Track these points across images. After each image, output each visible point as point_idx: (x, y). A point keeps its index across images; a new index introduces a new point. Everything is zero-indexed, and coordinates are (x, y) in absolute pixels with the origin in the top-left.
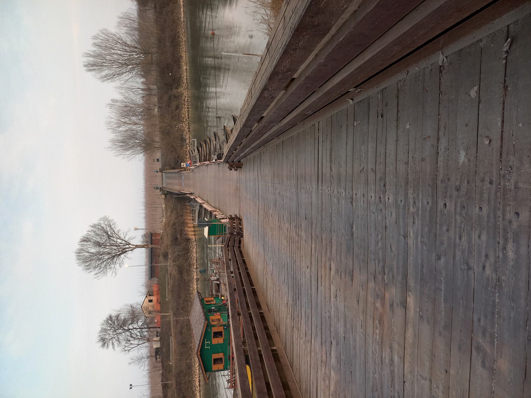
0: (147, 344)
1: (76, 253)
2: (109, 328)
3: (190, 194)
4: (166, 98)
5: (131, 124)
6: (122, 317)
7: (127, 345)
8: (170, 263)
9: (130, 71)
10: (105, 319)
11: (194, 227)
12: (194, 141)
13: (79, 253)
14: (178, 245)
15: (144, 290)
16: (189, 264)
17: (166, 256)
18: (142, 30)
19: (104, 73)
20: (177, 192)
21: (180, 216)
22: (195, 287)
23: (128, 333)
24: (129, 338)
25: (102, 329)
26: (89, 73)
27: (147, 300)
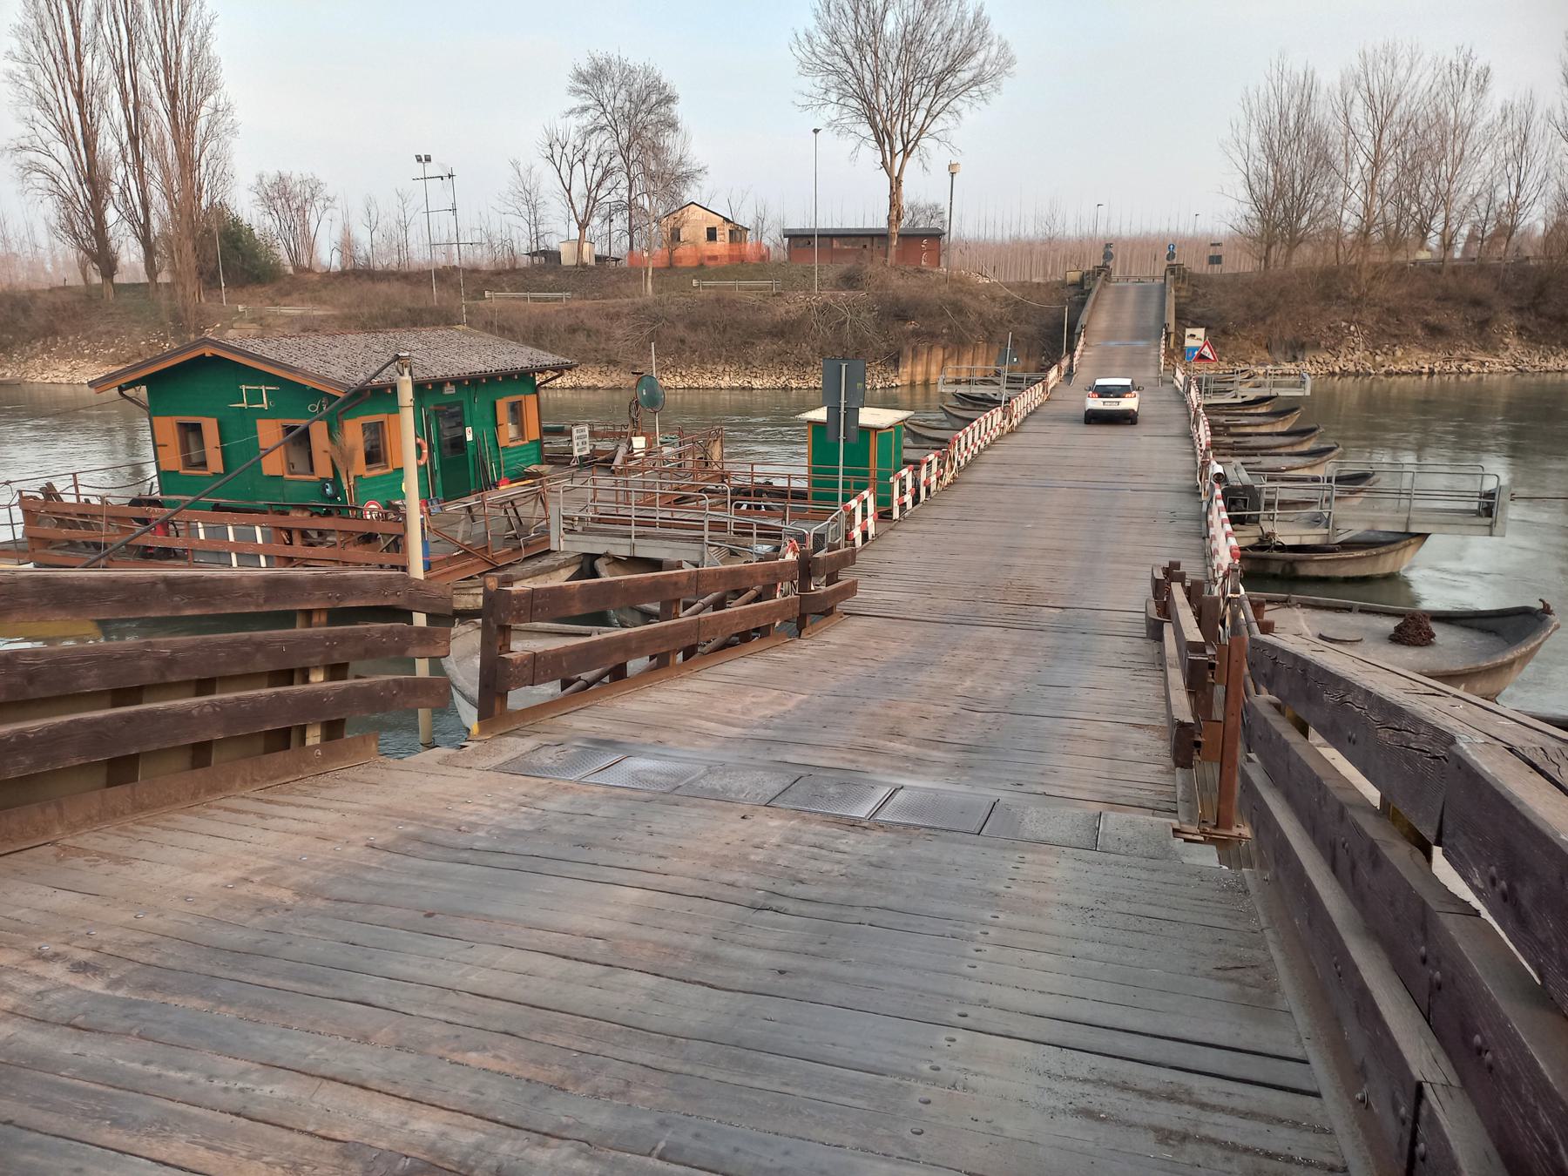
3: (1070, 367)
4: (1481, 286)
5: (1378, 144)
6: (669, 140)
7: (569, 149)
14: (878, 325)
16: (808, 363)
17: (850, 281)
20: (1083, 320)
21: (990, 332)
22: (725, 382)
27: (716, 222)
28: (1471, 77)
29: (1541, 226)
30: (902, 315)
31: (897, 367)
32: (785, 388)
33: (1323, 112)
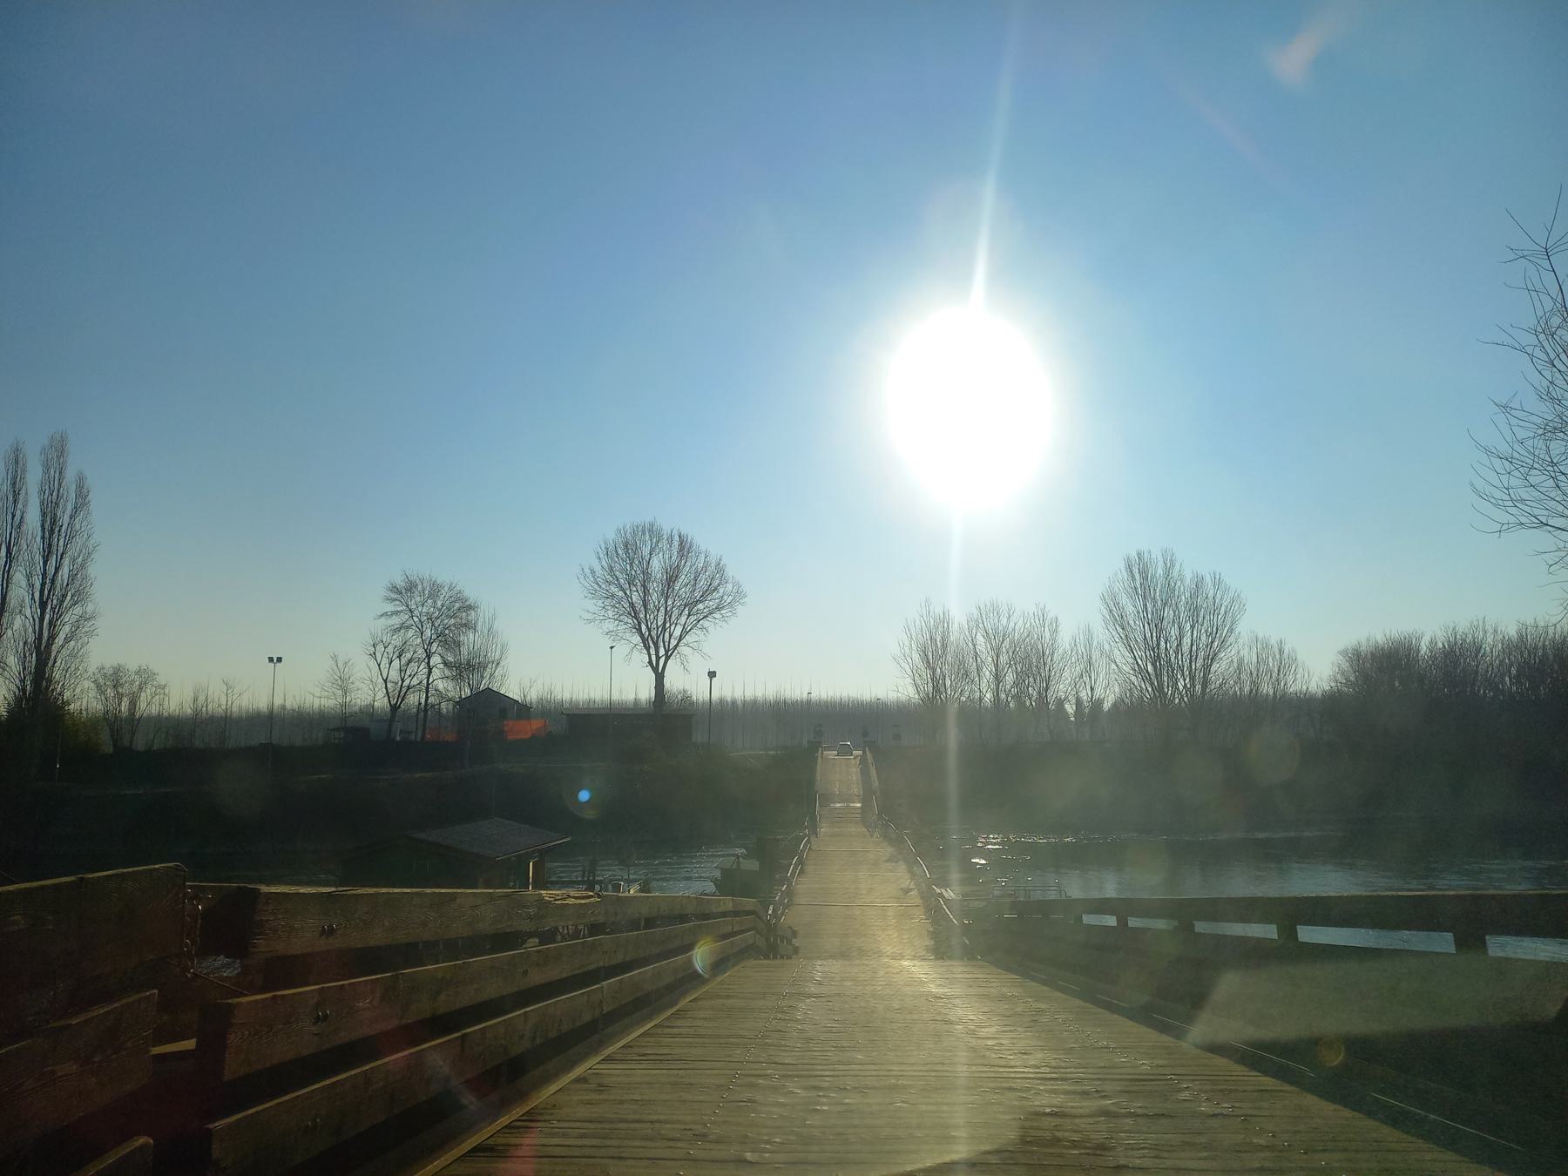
1: (652, 525)
9: (1140, 671)
13: (651, 531)
19: (1125, 600)
24: (409, 655)
25: (440, 587)
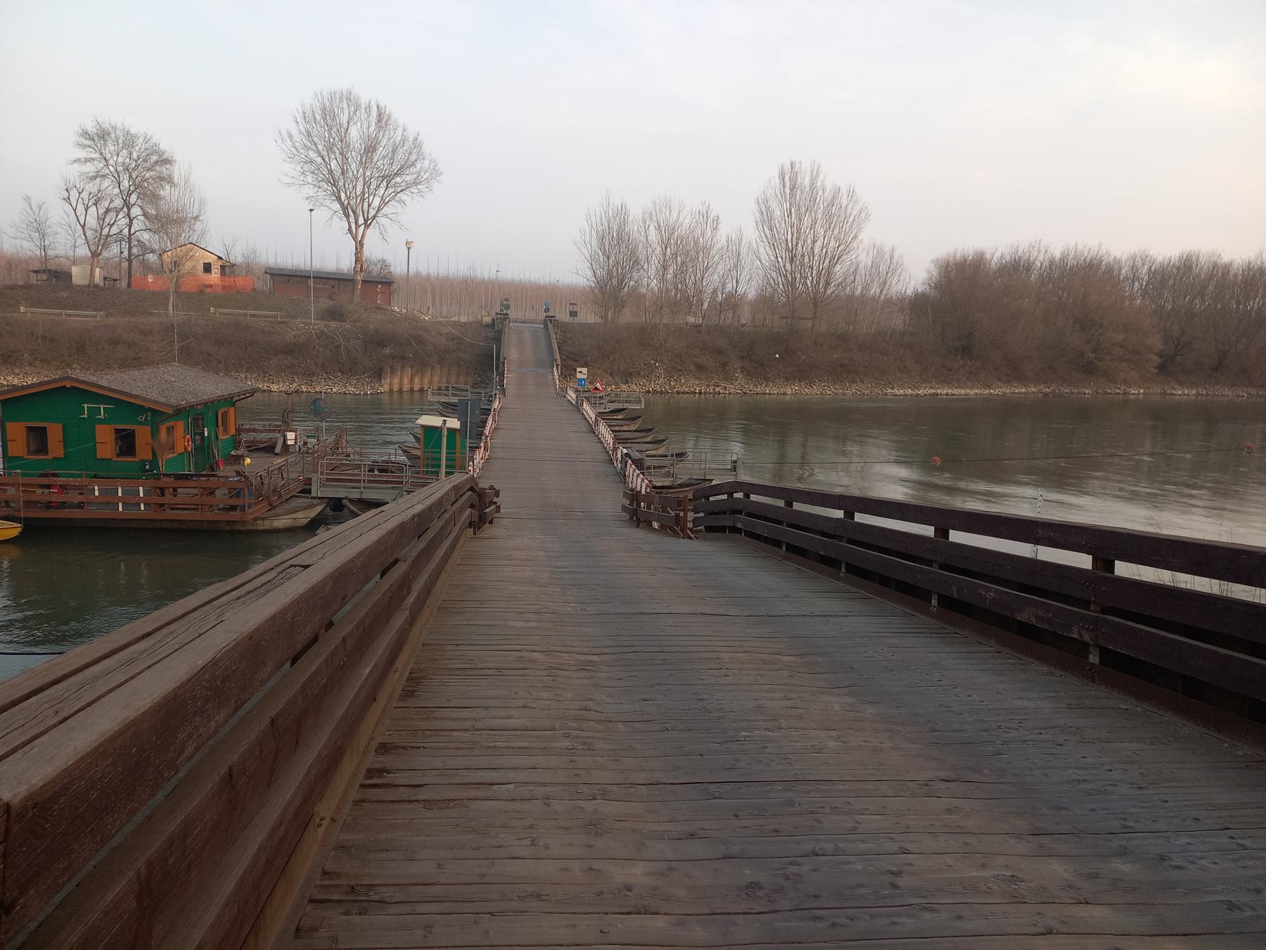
0: (83, 251)
2: (135, 155)
6: (165, 191)
7: (85, 195)
8: (316, 324)
10: (162, 147)
11: (422, 390)
12: (639, 402)
15: (237, 257)
16: (313, 374)
18: (855, 305)
23: (118, 203)
24: (105, 204)
26: (776, 173)
27: (211, 259)
28: (710, 220)
29: (754, 293)
30: (381, 344)
31: (380, 380)
32: (297, 392)
33: (634, 228)
